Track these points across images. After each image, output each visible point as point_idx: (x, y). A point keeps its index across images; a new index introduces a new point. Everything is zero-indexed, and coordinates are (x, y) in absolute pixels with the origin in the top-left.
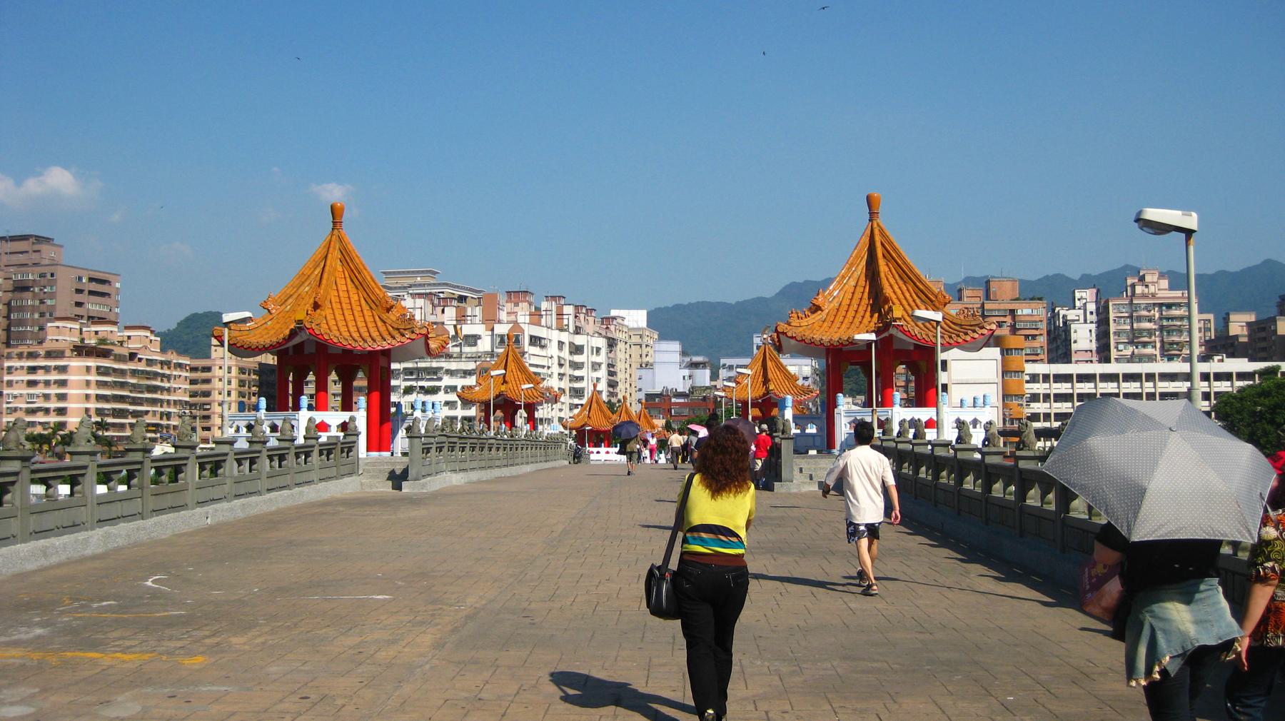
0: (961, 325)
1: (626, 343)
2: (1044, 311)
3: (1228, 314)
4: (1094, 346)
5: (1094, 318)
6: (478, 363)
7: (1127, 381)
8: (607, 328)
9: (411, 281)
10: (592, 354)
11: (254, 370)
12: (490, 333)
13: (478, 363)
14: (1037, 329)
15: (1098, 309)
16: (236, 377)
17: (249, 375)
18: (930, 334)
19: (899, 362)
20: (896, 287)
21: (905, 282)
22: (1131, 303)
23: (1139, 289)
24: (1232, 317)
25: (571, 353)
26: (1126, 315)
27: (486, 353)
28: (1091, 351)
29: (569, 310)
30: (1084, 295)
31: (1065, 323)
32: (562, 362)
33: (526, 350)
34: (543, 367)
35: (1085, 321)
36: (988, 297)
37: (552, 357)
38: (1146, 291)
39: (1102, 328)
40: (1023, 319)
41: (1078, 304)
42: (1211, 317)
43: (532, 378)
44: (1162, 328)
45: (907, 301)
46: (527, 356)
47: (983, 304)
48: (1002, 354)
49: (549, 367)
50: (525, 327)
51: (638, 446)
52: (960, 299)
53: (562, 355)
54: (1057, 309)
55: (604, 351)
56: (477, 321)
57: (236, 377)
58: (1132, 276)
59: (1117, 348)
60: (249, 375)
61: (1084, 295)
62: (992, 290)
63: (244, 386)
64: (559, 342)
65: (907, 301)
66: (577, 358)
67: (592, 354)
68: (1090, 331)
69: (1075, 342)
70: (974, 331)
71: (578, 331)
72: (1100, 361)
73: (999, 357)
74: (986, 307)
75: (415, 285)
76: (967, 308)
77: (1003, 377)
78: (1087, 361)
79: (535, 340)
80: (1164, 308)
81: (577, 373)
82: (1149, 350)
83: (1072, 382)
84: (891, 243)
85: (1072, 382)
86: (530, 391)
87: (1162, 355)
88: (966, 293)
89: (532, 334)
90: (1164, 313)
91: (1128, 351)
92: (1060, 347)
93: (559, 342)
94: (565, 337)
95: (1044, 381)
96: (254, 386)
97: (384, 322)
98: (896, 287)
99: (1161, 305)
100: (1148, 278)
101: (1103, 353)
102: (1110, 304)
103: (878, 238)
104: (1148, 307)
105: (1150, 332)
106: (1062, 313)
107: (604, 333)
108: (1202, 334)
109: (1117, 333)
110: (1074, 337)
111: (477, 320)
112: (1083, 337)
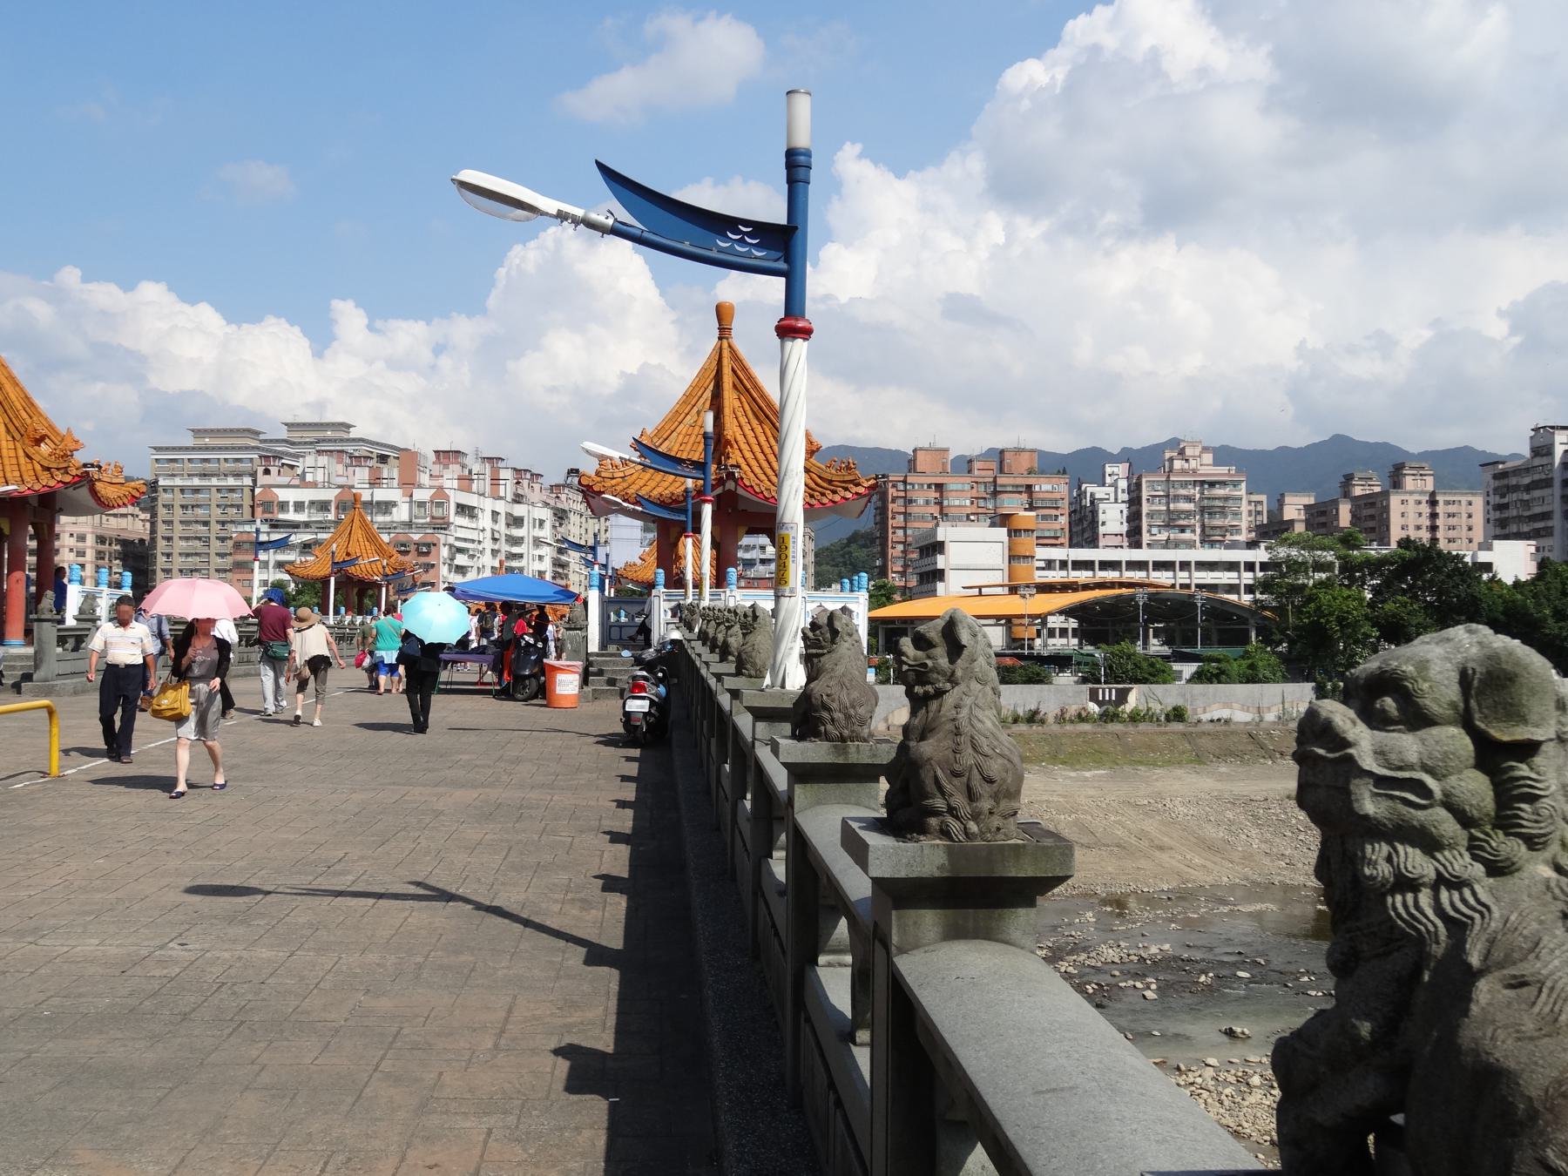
0: (832, 481)
1: (581, 515)
2: (1066, 487)
3: (1283, 495)
4: (1124, 528)
5: (1126, 497)
6: (392, 535)
7: (1159, 570)
8: (558, 497)
9: (320, 435)
10: (534, 527)
11: (116, 539)
12: (408, 499)
13: (392, 535)
14: (1057, 508)
15: (1129, 486)
16: (92, 548)
17: (110, 544)
18: (773, 488)
19: (746, 529)
20: (747, 428)
21: (761, 423)
22: (1168, 480)
23: (1178, 464)
24: (1288, 499)
25: (508, 525)
26: (1162, 493)
27: (404, 524)
28: (1121, 535)
29: (506, 474)
30: (1116, 470)
31: (1092, 502)
32: (497, 536)
33: (451, 521)
34: (473, 541)
35: (1116, 501)
36: (1001, 471)
37: (483, 530)
38: (1186, 466)
39: (1134, 508)
40: (1041, 495)
41: (1108, 480)
42: (1263, 498)
43: (383, 548)
44: (1203, 510)
45: (761, 447)
46: (452, 527)
47: (995, 478)
48: (1009, 535)
49: (480, 542)
50: (451, 493)
51: (1547, 612)
52: (970, 472)
53: (496, 527)
54: (1084, 486)
55: (548, 525)
56: (395, 485)
57: (92, 548)
58: (1172, 450)
59: (1149, 531)
60: (110, 544)
61: (1116, 470)
62: (1007, 461)
63: (103, 559)
64: (493, 511)
65: (761, 447)
66: (516, 532)
67: (534, 527)
68: (1122, 512)
69: (1104, 523)
70: (846, 489)
71: (518, 499)
72: (1130, 546)
73: (1006, 539)
74: (999, 481)
75: (324, 441)
76: (976, 482)
77: (1010, 562)
78: (1116, 547)
79: (463, 509)
80: (1206, 486)
81: (515, 550)
82: (1187, 535)
83: (1093, 569)
84: (745, 369)
85: (1093, 569)
86: (368, 566)
87: (1203, 542)
88: (977, 465)
89: (460, 502)
90: (1206, 492)
91: (1163, 536)
92: (1084, 527)
93: (493, 511)
94: (501, 507)
95: (1061, 569)
96: (116, 559)
97: (31, 459)
98: (747, 428)
99: (1203, 483)
100: (1189, 452)
101: (1134, 537)
102: (1144, 480)
103: (726, 362)
104: (1184, 484)
105: (1188, 514)
106: (1089, 490)
107: (552, 503)
108: (1252, 518)
109: (1151, 515)
110: (1101, 517)
111: (395, 483)
112: (1113, 518)
